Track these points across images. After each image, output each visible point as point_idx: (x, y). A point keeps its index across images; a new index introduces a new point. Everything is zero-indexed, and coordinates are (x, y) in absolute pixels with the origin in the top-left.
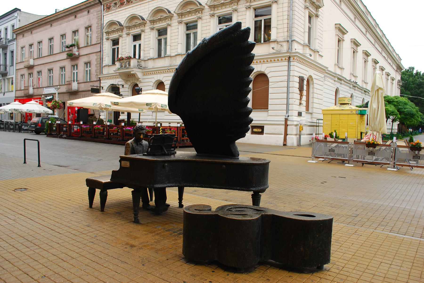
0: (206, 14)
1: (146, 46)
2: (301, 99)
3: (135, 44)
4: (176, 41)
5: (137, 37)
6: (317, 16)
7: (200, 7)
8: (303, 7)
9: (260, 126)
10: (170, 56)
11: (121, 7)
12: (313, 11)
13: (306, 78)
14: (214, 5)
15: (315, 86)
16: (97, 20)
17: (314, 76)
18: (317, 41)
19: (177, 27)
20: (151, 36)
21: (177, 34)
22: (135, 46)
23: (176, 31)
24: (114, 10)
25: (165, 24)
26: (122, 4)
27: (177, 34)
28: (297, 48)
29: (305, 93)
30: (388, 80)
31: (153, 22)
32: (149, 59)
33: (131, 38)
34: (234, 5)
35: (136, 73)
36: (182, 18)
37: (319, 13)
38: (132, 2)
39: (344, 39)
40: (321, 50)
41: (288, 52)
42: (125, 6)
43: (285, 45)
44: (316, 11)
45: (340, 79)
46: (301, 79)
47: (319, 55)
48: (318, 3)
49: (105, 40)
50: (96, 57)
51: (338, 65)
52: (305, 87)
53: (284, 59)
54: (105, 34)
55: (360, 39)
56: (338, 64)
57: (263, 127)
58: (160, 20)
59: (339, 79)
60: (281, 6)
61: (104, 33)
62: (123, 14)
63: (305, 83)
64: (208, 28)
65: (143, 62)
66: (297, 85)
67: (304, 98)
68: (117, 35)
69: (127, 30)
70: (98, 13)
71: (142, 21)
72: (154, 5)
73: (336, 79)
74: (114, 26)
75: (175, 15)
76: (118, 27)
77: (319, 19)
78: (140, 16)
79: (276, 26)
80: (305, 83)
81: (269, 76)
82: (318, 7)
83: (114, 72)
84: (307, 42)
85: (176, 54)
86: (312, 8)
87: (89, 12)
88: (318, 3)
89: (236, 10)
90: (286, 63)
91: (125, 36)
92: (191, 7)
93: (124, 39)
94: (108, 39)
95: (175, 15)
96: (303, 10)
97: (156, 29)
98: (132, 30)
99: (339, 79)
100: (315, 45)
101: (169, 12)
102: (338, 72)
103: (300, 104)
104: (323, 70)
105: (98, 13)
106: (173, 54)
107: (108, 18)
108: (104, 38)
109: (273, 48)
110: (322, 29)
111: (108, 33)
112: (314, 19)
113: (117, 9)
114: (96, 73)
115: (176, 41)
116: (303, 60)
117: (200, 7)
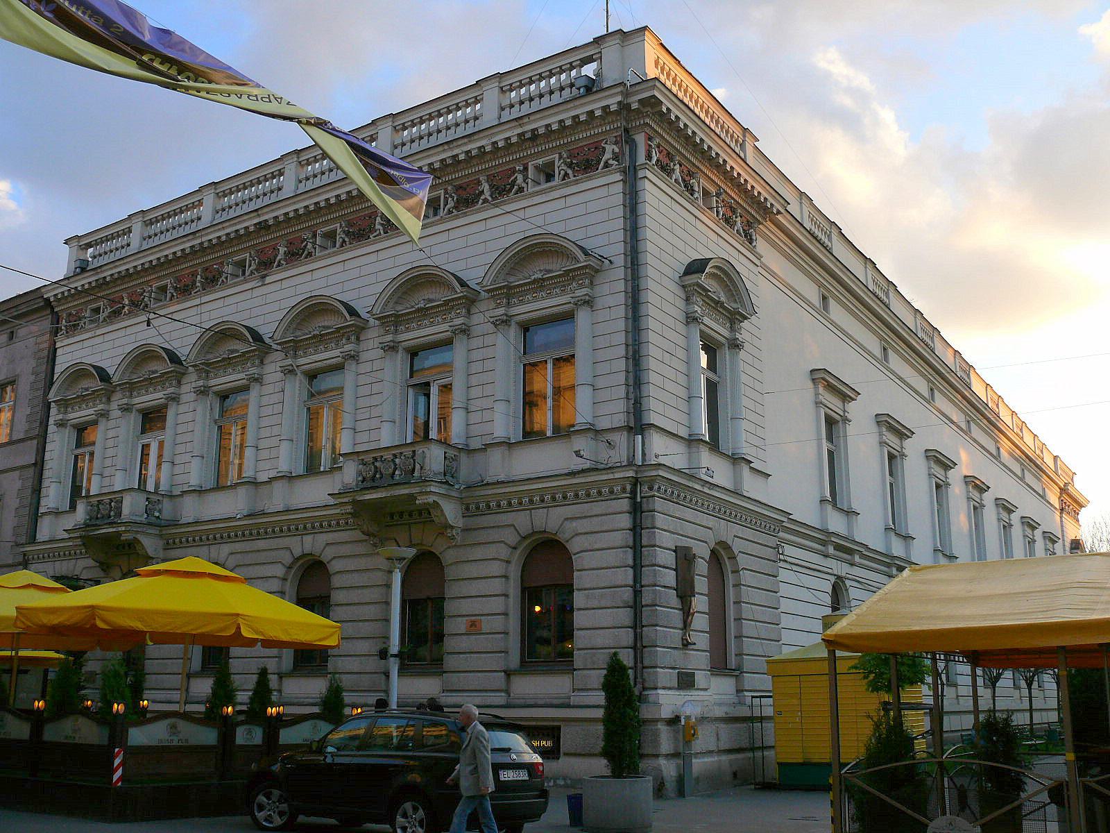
0: (371, 344)
1: (180, 449)
2: (686, 625)
3: (146, 441)
4: (276, 430)
5: (152, 419)
6: (735, 345)
7: (583, 261)
8: (682, 317)
9: (547, 728)
10: (254, 483)
11: (112, 323)
12: (719, 329)
13: (702, 552)
14: (397, 316)
15: (746, 577)
16: (33, 363)
17: (737, 546)
18: (744, 425)
19: (279, 386)
20: (199, 418)
21: (278, 408)
22: (145, 448)
23: (276, 398)
24: (90, 330)
25: (445, 327)
26: (116, 314)
27: (278, 408)
28: (665, 451)
29: (700, 603)
30: (1032, 542)
31: (393, 321)
32: (184, 492)
33: (134, 420)
34: (581, 286)
35: (138, 536)
36: (295, 356)
37: (743, 336)
38: (146, 306)
39: (849, 417)
40: (761, 454)
41: (631, 464)
42: (123, 320)
43: (621, 439)
44: (732, 329)
45: (847, 549)
46: (684, 558)
47: (751, 468)
48: (735, 306)
49: (52, 428)
50: (18, 484)
51: (835, 505)
52: (701, 584)
53: (617, 489)
54: (53, 411)
55: (907, 411)
56: (834, 498)
57: (559, 728)
58: (424, 313)
59: (838, 547)
60: (601, 315)
61: (53, 405)
62: (117, 343)
63: (702, 567)
64: (376, 388)
65: (166, 500)
66: (670, 578)
67: (700, 622)
68: (91, 411)
69: (200, 378)
70: (39, 340)
71: (170, 367)
72: (300, 289)
73: (831, 550)
74: (85, 383)
75: (372, 321)
76: (95, 384)
77: (742, 354)
78: (94, 367)
79: (590, 380)
80: (702, 567)
81: (574, 546)
82: (735, 318)
83: (66, 536)
84: (704, 429)
85: (273, 474)
86: (716, 321)
87: (11, 336)
88: (735, 306)
89: (353, 357)
90: (282, 576)
91: (116, 413)
92: (326, 324)
93: (112, 423)
94: (61, 424)
95: (372, 321)
96: (681, 328)
97: (139, 411)
98: (305, 355)
99: (838, 547)
100: (743, 439)
101: (353, 312)
102: (836, 523)
103: (686, 644)
104: (775, 524)
105: (39, 340)
106: (263, 477)
107: (69, 357)
108: (51, 421)
109: (578, 454)
110: (758, 386)
111: (65, 404)
112: (725, 355)
113: (98, 327)
114: (14, 538)
115: (276, 430)
116: (687, 489)
117: (351, 321)
